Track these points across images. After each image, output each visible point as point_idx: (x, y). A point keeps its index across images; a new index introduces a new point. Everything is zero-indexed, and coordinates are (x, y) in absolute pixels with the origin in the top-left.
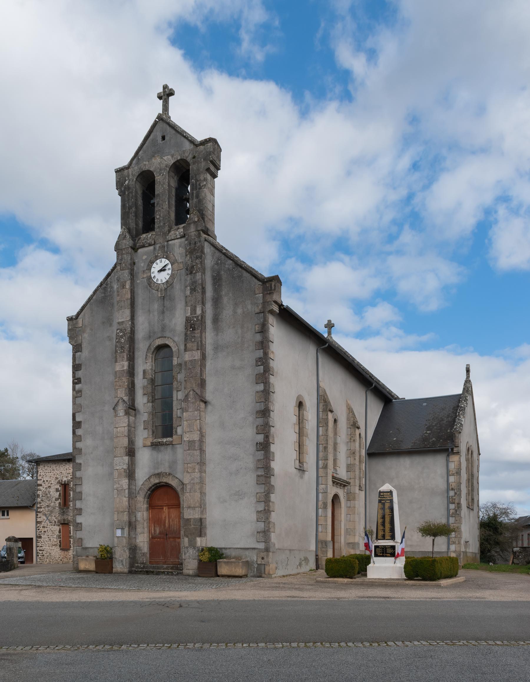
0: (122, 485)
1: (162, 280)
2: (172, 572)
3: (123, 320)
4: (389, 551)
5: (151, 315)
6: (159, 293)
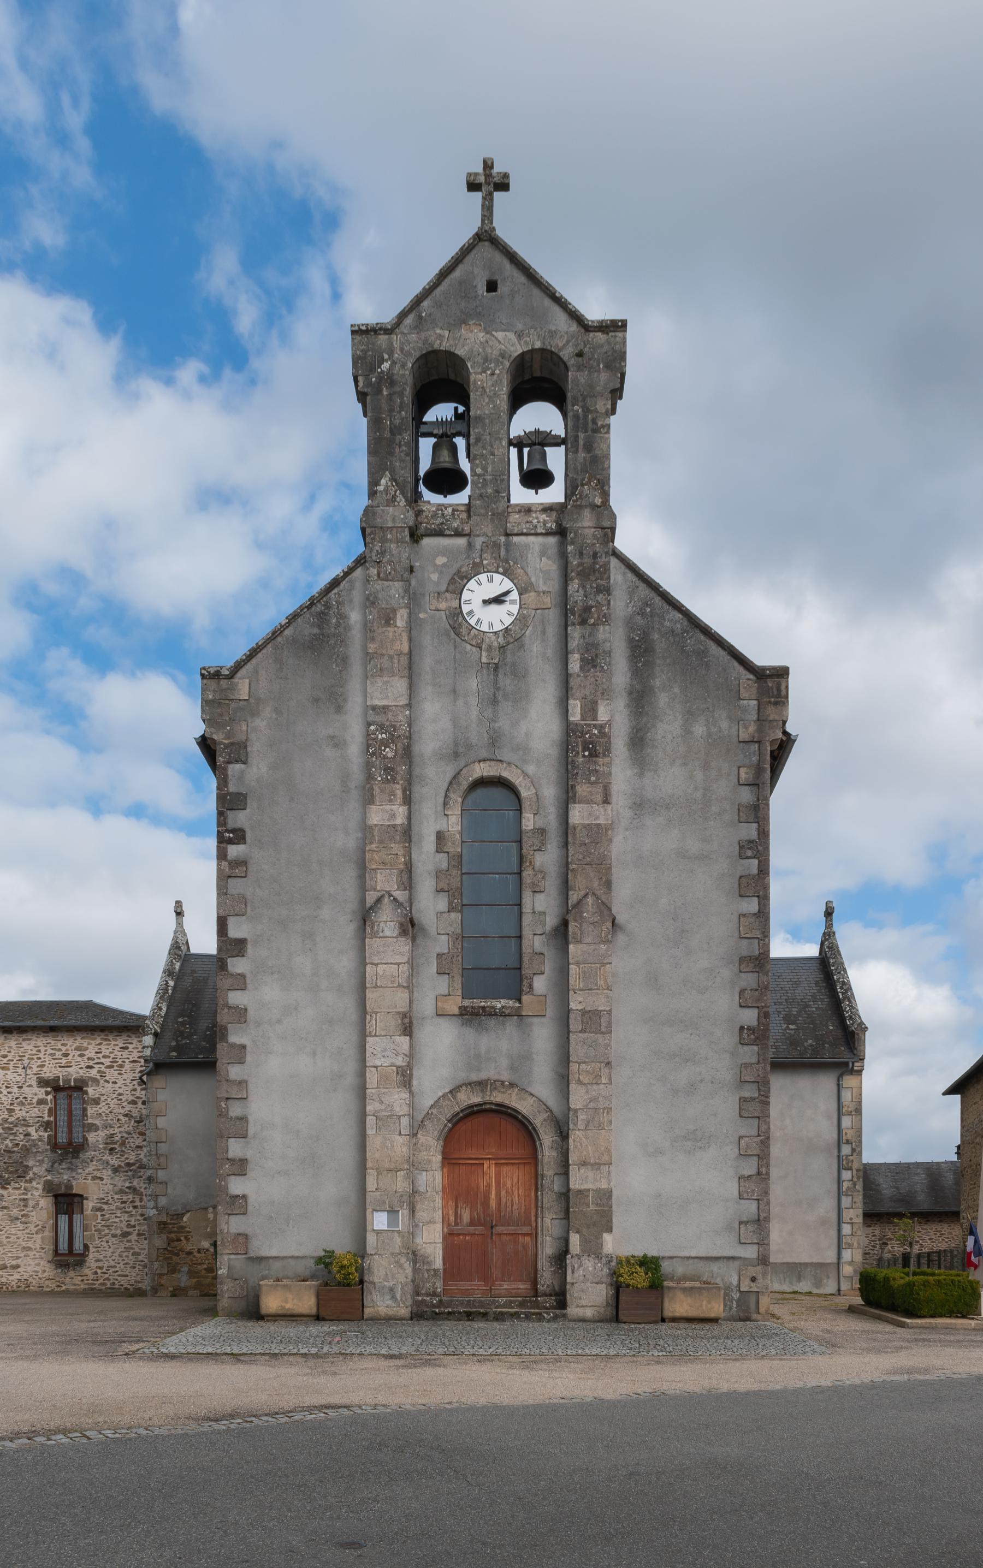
0: (391, 1106)
1: (491, 625)
2: (540, 1314)
3: (385, 702)
5: (460, 703)
6: (484, 654)
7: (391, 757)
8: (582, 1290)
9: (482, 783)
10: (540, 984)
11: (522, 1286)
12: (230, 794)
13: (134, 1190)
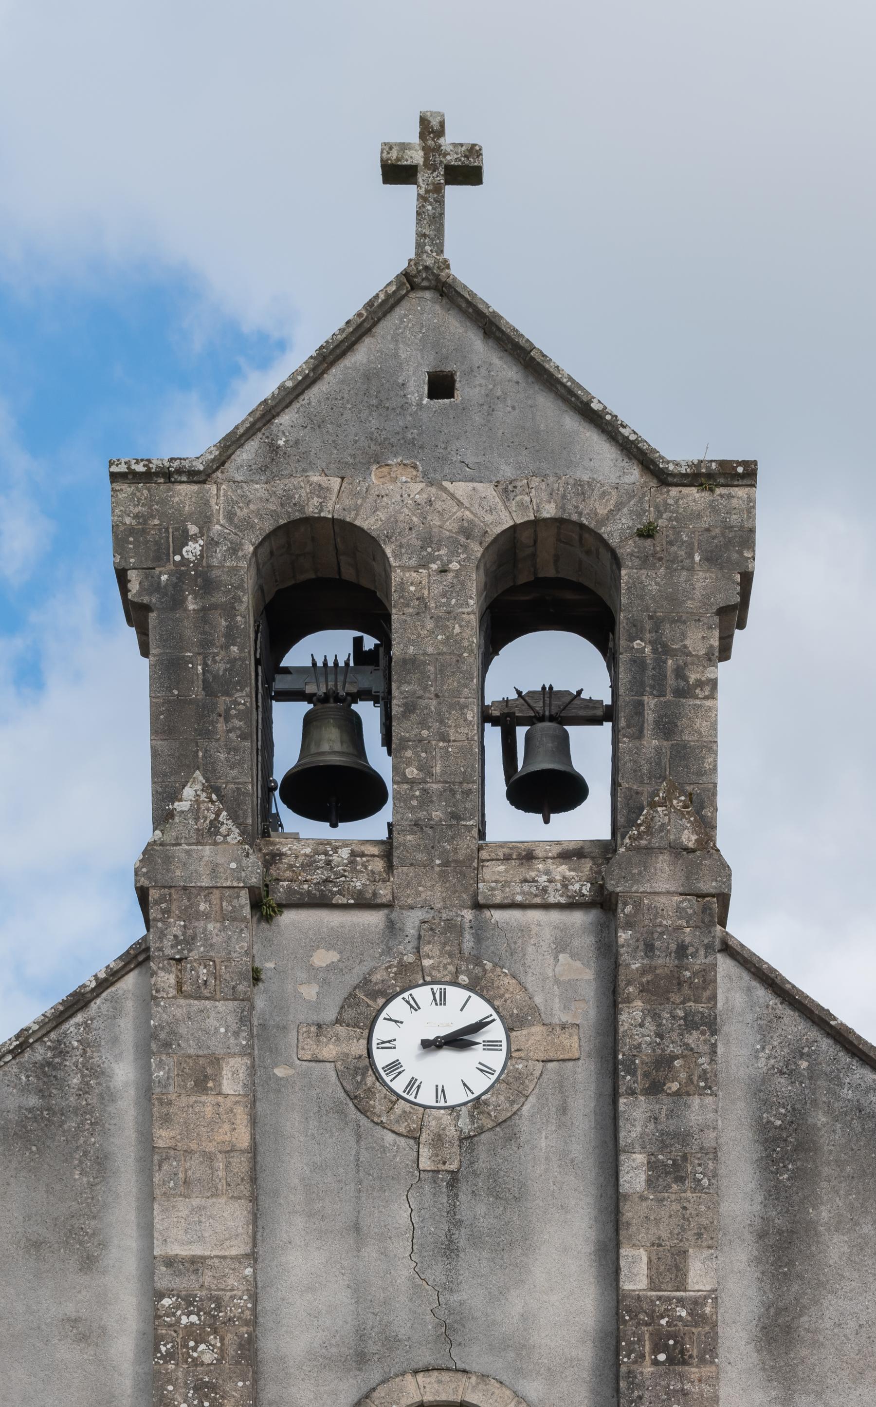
1: (441, 1092)
5: (370, 1252)
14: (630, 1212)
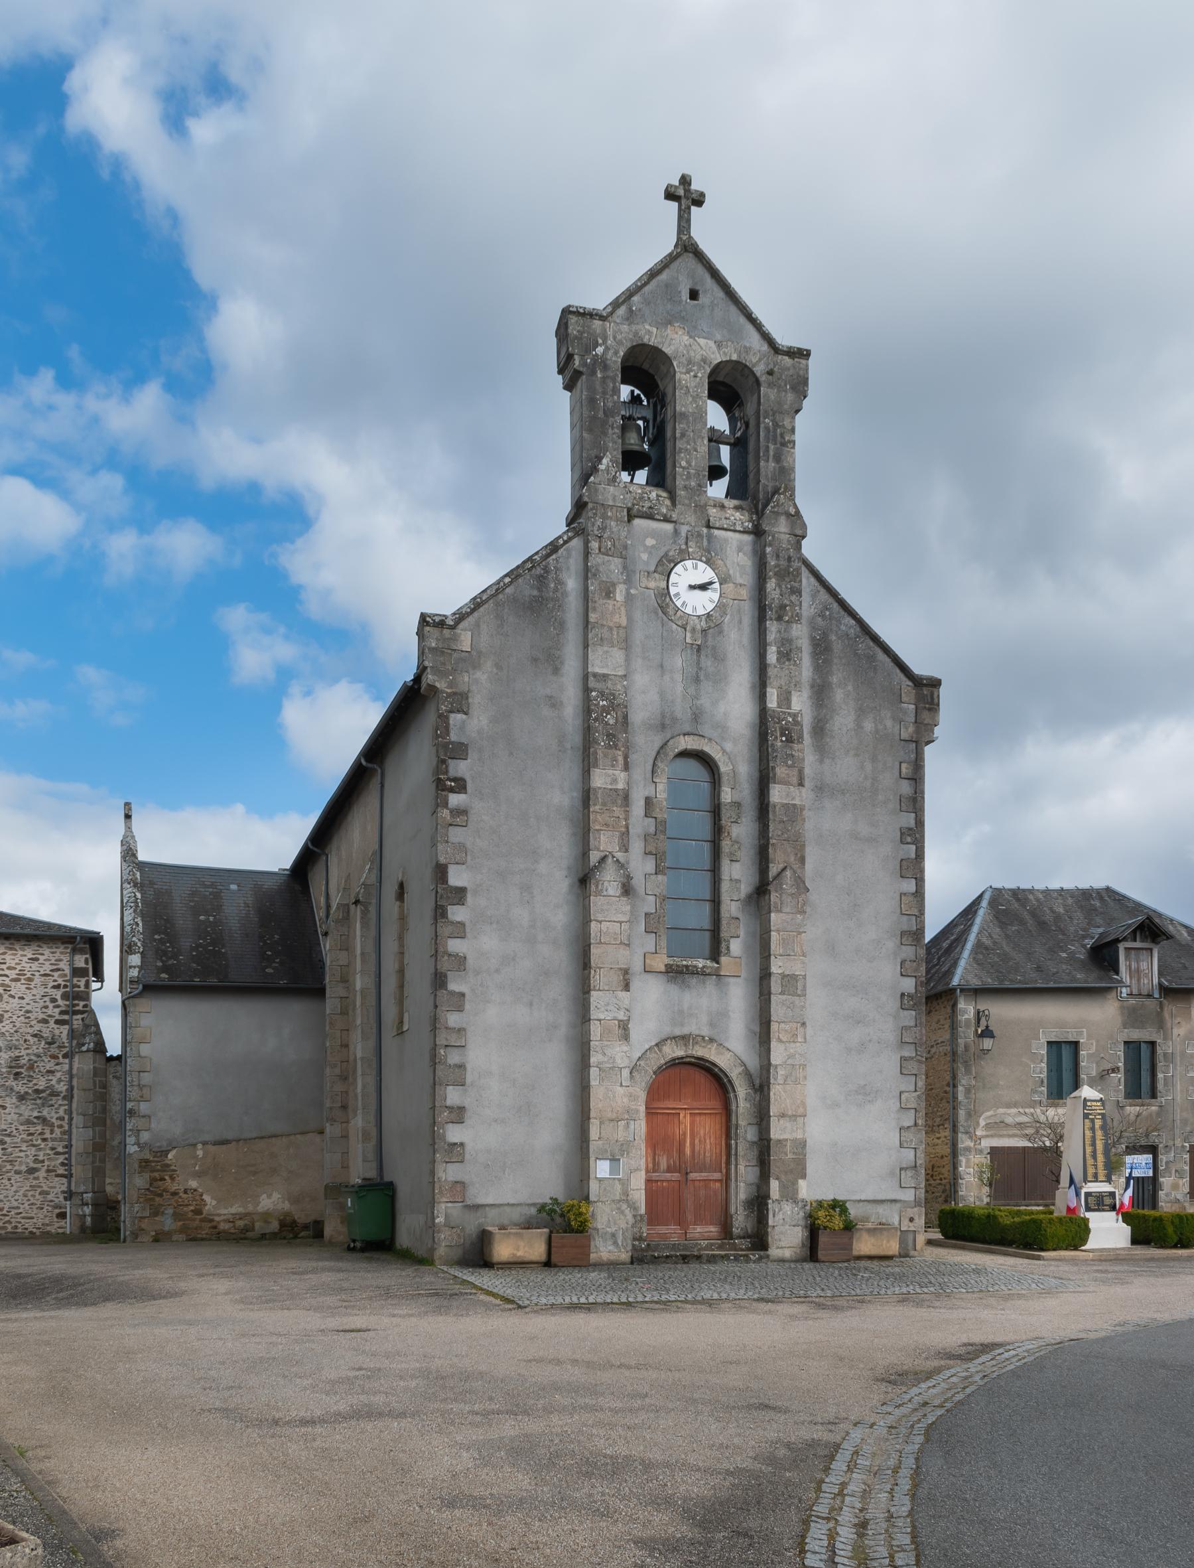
1: (695, 609)
2: (747, 1256)
3: (605, 671)
4: (1108, 1201)
5: (667, 677)
6: (688, 635)
7: (600, 725)
8: (782, 1233)
9: (685, 754)
10: (736, 947)
11: (713, 1229)
12: (452, 743)
13: (44, 1121)
14: (771, 672)
